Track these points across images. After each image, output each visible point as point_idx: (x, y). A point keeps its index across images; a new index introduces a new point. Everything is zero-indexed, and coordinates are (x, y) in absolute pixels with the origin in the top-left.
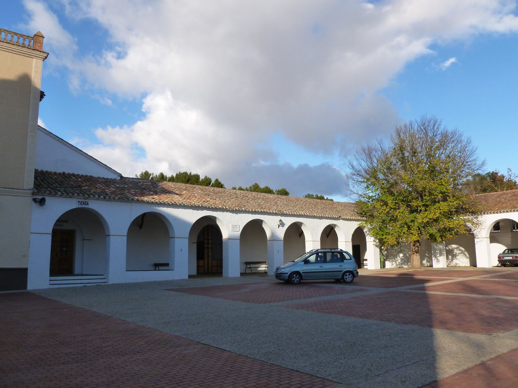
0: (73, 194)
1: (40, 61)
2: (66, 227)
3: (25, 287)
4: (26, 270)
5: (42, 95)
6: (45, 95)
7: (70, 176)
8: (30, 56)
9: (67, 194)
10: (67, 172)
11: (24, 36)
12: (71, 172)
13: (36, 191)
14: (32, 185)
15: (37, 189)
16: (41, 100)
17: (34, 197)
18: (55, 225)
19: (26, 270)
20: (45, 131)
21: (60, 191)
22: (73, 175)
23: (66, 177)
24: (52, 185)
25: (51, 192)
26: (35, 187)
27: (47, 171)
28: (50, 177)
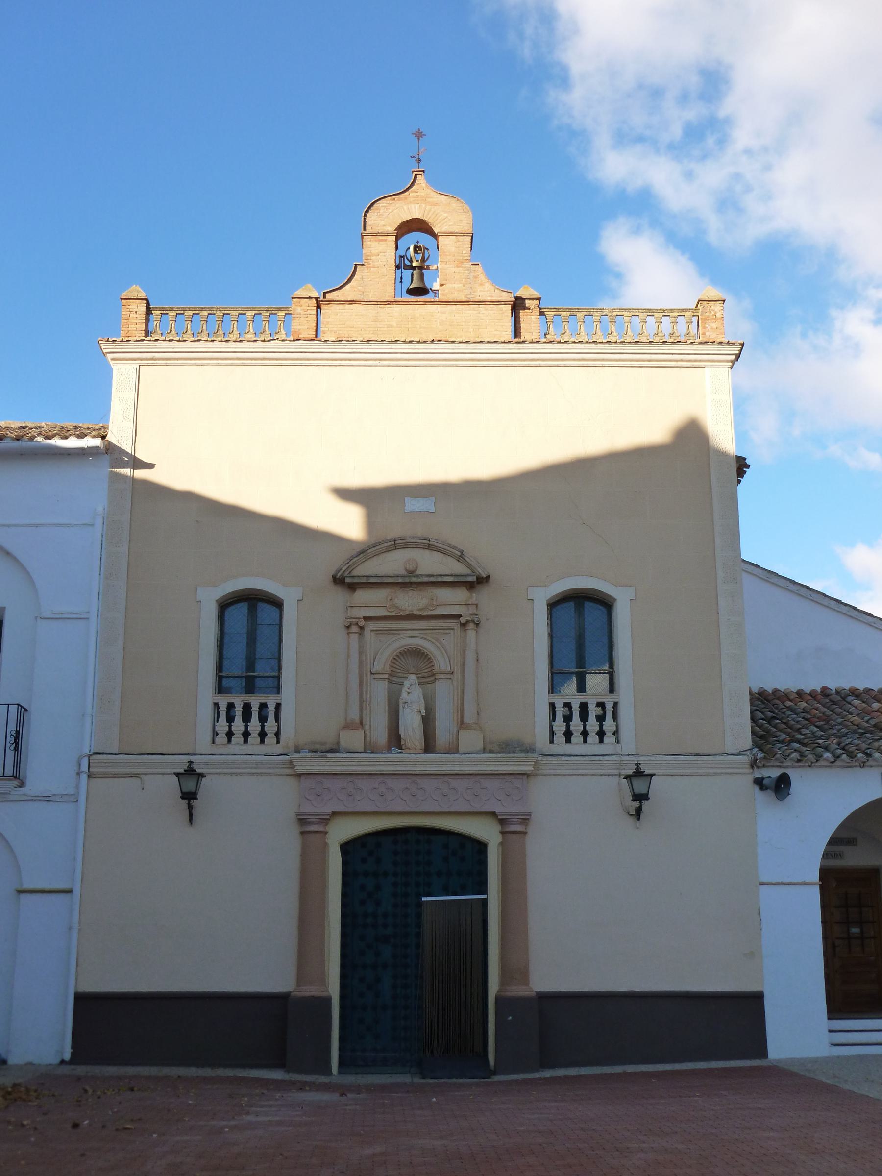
0: (869, 755)
1: (723, 373)
2: (856, 858)
3: (762, 1052)
4: (758, 997)
5: (741, 466)
6: (748, 466)
7: (844, 699)
8: (695, 365)
9: (852, 755)
10: (833, 685)
11: (672, 310)
12: (846, 684)
13: (760, 755)
14: (746, 740)
15: (761, 750)
16: (739, 482)
17: (758, 774)
18: (826, 855)
19: (758, 997)
20: (756, 570)
21: (826, 749)
22: (854, 693)
23: (834, 703)
24: (798, 731)
25: (802, 755)
26: (755, 744)
27: (776, 691)
28: (790, 709)
